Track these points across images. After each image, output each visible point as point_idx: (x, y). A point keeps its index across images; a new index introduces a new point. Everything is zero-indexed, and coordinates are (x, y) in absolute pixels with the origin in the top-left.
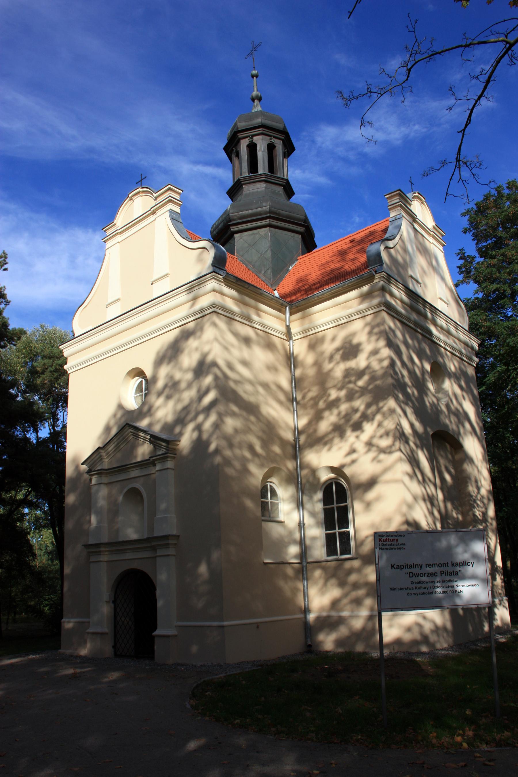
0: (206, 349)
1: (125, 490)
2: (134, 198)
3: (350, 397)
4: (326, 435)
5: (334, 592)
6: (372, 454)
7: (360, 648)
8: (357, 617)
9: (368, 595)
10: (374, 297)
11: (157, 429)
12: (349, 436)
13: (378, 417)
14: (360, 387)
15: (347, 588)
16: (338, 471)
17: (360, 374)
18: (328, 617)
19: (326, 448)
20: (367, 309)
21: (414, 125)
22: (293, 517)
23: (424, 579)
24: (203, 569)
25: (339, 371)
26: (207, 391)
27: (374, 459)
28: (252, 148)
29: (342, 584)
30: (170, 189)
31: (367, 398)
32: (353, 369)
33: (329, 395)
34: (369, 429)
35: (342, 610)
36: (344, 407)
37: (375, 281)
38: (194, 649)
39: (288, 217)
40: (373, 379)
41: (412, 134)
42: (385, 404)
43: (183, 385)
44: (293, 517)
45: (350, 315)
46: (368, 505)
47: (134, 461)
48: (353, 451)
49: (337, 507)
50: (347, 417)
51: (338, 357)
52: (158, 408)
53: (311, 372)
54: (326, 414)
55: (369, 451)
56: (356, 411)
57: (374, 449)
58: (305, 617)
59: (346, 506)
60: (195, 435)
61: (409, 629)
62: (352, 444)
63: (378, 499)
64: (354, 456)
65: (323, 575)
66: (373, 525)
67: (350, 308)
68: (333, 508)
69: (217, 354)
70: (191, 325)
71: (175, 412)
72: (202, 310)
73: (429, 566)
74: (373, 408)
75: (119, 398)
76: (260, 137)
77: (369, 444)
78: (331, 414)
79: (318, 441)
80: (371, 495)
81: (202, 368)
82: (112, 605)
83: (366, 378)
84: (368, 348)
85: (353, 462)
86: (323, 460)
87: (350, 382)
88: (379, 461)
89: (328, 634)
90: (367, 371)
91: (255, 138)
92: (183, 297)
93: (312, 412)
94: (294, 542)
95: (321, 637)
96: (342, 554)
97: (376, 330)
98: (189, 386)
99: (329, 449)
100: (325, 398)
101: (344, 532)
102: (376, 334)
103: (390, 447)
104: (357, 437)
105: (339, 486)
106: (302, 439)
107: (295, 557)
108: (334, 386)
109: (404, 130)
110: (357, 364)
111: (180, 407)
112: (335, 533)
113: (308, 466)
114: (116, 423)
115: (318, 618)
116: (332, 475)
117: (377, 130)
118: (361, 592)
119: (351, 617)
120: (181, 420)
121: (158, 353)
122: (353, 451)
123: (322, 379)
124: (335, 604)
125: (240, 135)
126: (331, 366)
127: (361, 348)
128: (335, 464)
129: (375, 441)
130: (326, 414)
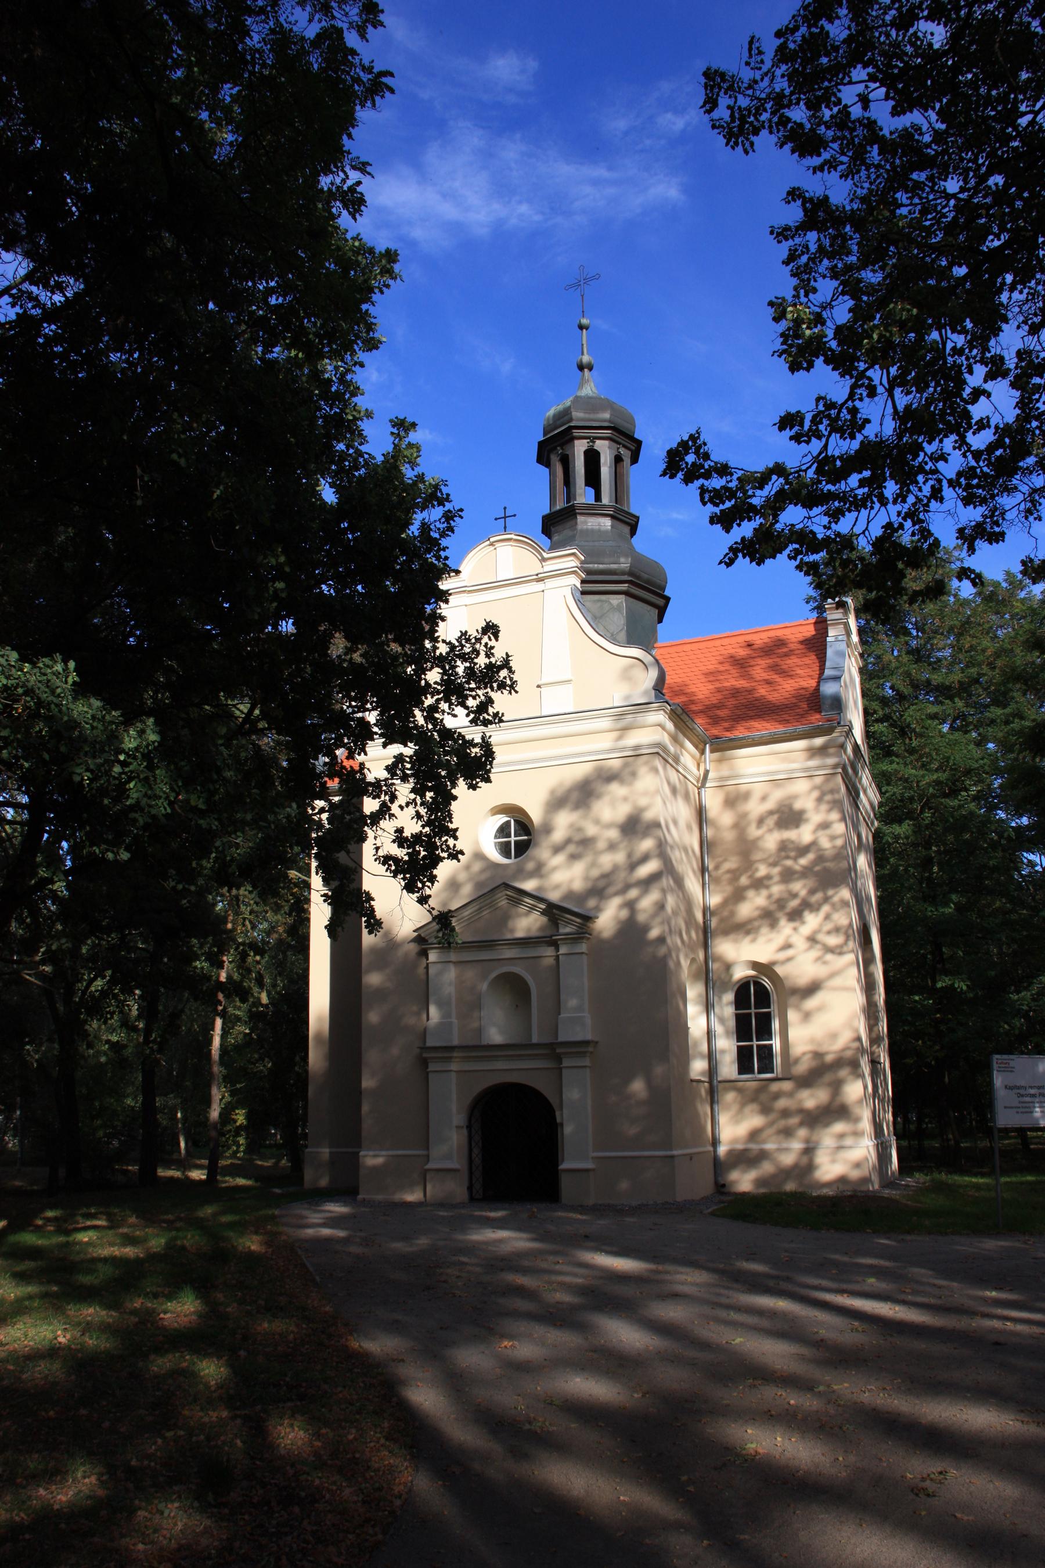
0: (643, 802)
1: (494, 975)
2: (497, 545)
3: (788, 876)
4: (750, 921)
5: (754, 1121)
6: (815, 953)
7: (790, 1187)
8: (787, 1150)
9: (801, 1124)
10: (828, 755)
11: (554, 896)
12: (784, 927)
13: (826, 908)
14: (802, 866)
15: (772, 1116)
16: (764, 969)
17: (803, 850)
18: (746, 1150)
19: (749, 938)
20: (818, 768)
21: (520, 202)
22: (706, 1025)
23: (1028, 1099)
24: (638, 1086)
25: (771, 841)
26: (645, 859)
27: (818, 959)
28: (592, 458)
29: (765, 1110)
30: (573, 554)
31: (810, 883)
32: (793, 842)
33: (757, 870)
34: (812, 921)
35: (764, 1142)
36: (777, 889)
37: (834, 735)
38: (624, 1185)
39: (648, 582)
40: (820, 859)
41: (514, 221)
42: (836, 893)
43: (601, 845)
44: (706, 1025)
45: (793, 771)
46: (807, 1016)
47: (509, 936)
48: (787, 946)
49: (756, 1014)
50: (781, 903)
51: (771, 822)
52: (555, 869)
53: (729, 836)
54: (751, 893)
55: (810, 948)
56: (795, 896)
57: (819, 946)
58: (715, 1151)
59: (770, 1013)
60: (624, 914)
61: (858, 1165)
62: (789, 937)
63: (820, 1009)
64: (789, 953)
65: (739, 1099)
66: (812, 1041)
67: (793, 762)
68: (750, 1014)
69: (656, 810)
70: (616, 764)
71: (586, 878)
72: (637, 747)
73: (1031, 1087)
74: (819, 896)
75: (477, 843)
76: (606, 442)
77: (812, 940)
78: (759, 895)
79: (744, 929)
80: (811, 1003)
81: (633, 826)
82: (465, 1132)
83: (811, 856)
84: (815, 818)
85: (789, 959)
86: (742, 955)
87: (788, 857)
88: (825, 963)
89: (744, 1171)
90: (814, 849)
91: (598, 442)
92: (605, 723)
93: (729, 889)
94: (702, 1056)
95: (734, 1175)
96: (759, 1072)
97: (828, 797)
98: (612, 847)
99: (754, 941)
100: (749, 873)
101: (765, 1046)
102: (828, 802)
103: (841, 946)
104: (795, 929)
105: (759, 985)
106: (714, 923)
107: (703, 1074)
108: (763, 861)
109: (498, 209)
110: (799, 835)
111: (595, 873)
112: (752, 1046)
113: (718, 959)
114: (470, 879)
115: (731, 1153)
116: (752, 973)
117: (444, 196)
118: (794, 1121)
119: (780, 1150)
120: (599, 889)
121: (552, 792)
122: (787, 946)
123: (746, 848)
124: (754, 1135)
125: (576, 433)
126: (758, 833)
127: (805, 816)
128: (763, 958)
129: (820, 937)
130: (751, 893)
